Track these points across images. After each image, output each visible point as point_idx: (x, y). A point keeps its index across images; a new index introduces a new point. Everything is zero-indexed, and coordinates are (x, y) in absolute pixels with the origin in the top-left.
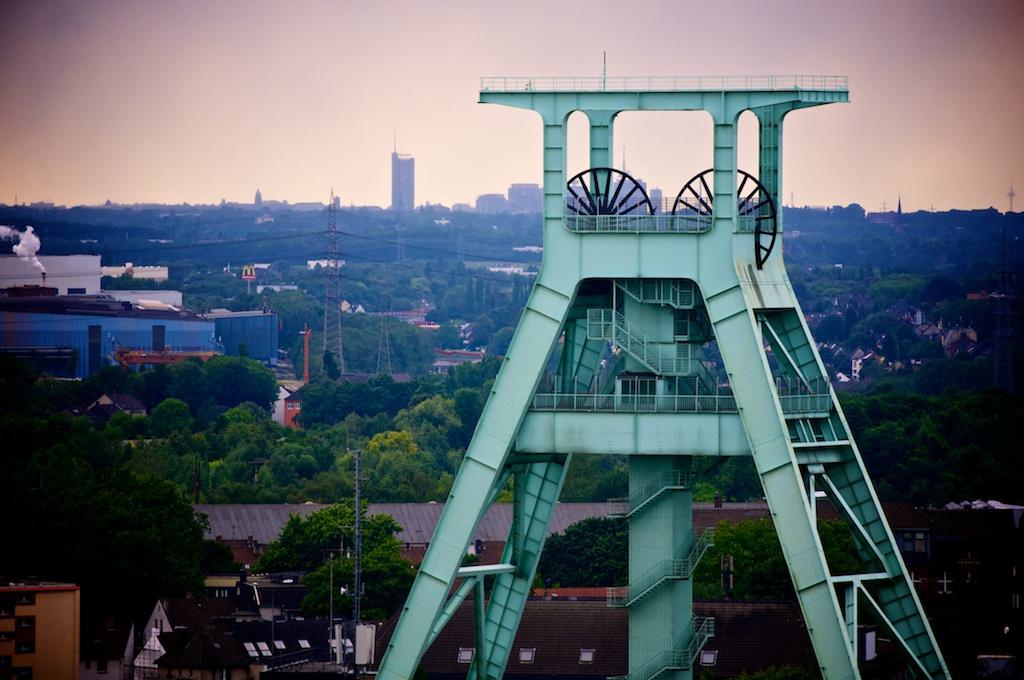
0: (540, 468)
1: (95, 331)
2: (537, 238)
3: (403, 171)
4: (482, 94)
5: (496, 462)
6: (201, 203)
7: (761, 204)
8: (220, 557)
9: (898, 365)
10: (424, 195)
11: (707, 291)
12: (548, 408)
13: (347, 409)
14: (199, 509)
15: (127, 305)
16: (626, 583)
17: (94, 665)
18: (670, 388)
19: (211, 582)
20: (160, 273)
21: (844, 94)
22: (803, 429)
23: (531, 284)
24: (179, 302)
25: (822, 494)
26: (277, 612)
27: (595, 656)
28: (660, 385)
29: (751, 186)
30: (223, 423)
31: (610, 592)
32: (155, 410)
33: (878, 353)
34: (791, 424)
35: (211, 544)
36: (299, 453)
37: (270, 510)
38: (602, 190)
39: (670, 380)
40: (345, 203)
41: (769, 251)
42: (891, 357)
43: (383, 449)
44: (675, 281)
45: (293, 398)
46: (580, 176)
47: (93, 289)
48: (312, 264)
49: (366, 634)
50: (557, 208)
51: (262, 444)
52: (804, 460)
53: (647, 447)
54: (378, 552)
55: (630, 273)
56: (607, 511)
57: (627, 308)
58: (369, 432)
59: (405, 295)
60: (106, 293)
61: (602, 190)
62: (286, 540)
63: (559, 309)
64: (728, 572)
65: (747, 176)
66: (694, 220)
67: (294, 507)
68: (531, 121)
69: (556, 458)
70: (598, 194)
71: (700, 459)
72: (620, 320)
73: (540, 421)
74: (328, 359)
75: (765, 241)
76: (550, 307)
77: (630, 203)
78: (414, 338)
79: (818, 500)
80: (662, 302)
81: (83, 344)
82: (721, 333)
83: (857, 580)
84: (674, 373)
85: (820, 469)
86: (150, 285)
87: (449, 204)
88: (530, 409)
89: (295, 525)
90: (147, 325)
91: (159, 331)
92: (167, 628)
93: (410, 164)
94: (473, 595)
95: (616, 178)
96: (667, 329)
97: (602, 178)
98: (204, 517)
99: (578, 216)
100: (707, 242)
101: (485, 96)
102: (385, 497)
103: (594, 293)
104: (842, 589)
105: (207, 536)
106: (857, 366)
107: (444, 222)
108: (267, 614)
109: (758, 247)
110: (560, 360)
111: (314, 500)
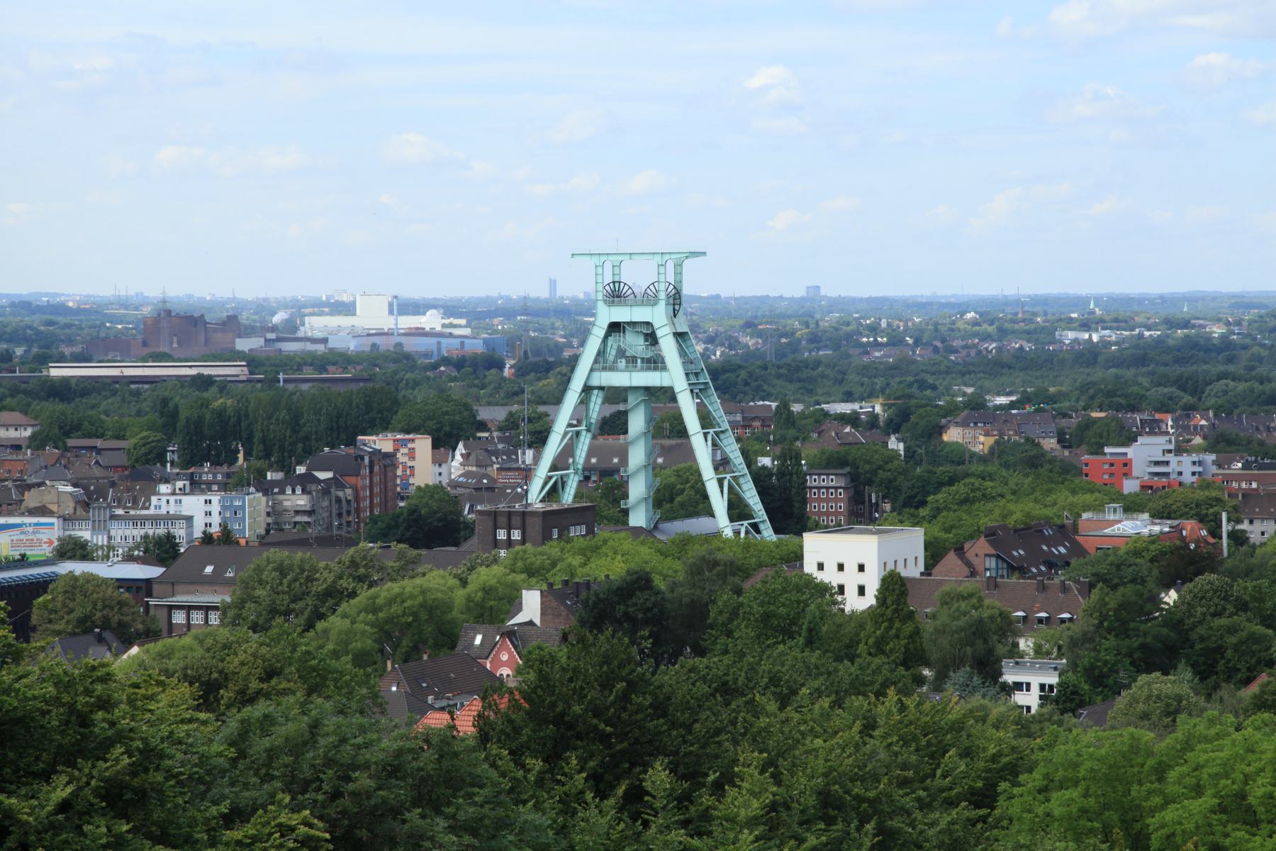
0: (595, 392)
1: (439, 343)
2: (595, 307)
3: (553, 283)
10: (559, 293)
11: (656, 326)
12: (598, 370)
13: (531, 371)
16: (626, 432)
18: (643, 362)
20: (463, 322)
21: (704, 254)
22: (692, 377)
28: (639, 361)
29: (671, 287)
30: (485, 376)
31: (622, 437)
34: (687, 374)
37: (501, 408)
39: (643, 359)
42: (731, 349)
44: (644, 323)
45: (511, 367)
47: (439, 328)
49: (530, 454)
50: (600, 296)
51: (500, 384)
53: (635, 384)
54: (541, 423)
56: (621, 407)
57: (627, 332)
58: (539, 379)
62: (507, 420)
63: (602, 333)
68: (590, 262)
69: (601, 388)
71: (655, 388)
73: (596, 374)
74: (525, 352)
76: (599, 332)
81: (435, 349)
82: (661, 341)
83: (711, 431)
86: (460, 326)
88: (592, 370)
89: (511, 415)
90: (458, 341)
91: (462, 343)
92: (464, 452)
93: (555, 281)
94: (571, 438)
95: (622, 285)
96: (641, 340)
97: (617, 285)
100: (655, 308)
101: (704, 254)
102: (545, 403)
103: (615, 327)
104: (705, 435)
105: (478, 418)
106: (718, 353)
108: (500, 446)
109: (674, 309)
110: (601, 353)
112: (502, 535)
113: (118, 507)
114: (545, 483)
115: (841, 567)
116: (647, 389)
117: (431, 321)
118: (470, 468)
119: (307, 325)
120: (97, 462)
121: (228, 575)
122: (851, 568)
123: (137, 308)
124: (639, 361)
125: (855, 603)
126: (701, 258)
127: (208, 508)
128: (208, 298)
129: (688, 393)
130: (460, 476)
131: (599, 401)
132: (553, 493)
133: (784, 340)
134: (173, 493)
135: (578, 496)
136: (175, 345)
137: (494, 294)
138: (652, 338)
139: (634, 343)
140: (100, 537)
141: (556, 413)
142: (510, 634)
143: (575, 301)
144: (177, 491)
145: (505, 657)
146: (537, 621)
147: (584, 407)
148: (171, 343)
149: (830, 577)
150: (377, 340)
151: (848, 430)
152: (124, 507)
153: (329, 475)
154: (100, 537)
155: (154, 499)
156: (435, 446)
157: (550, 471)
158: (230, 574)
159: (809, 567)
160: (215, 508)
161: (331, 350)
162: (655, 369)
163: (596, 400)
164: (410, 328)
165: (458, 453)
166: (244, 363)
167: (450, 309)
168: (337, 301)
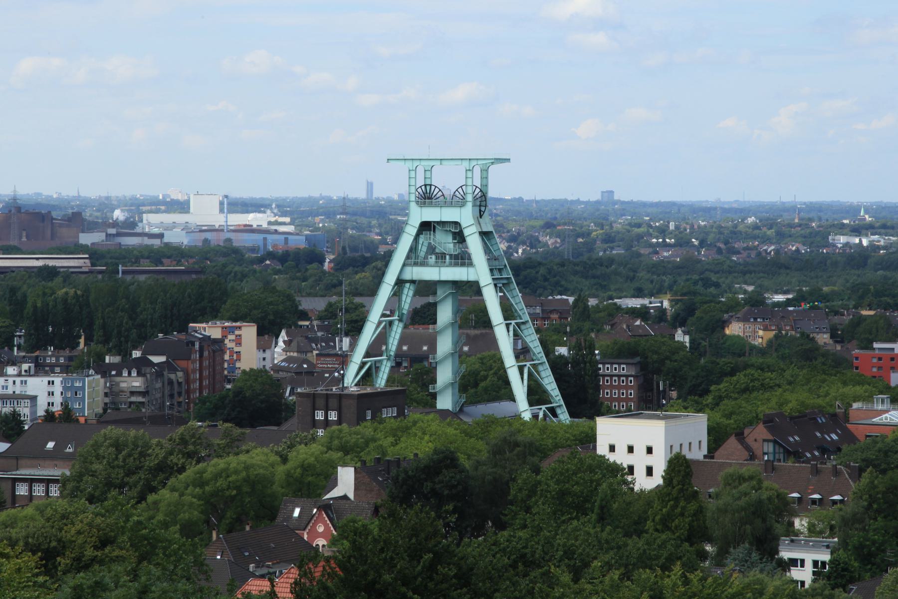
0: (407, 285)
1: (265, 239)
4: (388, 159)
5: (393, 283)
6: (328, 195)
7: (481, 196)
8: (304, 315)
9: (534, 251)
10: (376, 194)
11: (463, 225)
12: (410, 265)
14: (297, 299)
15: (276, 230)
16: (435, 322)
17: (261, 351)
19: (301, 323)
21: (508, 160)
22: (495, 272)
23: (406, 223)
24: (294, 229)
25: (502, 294)
26: (322, 333)
27: (428, 348)
28: (448, 257)
30: (307, 270)
32: (284, 266)
33: (527, 246)
35: (301, 311)
36: (332, 280)
37: (321, 299)
38: (428, 192)
39: (451, 255)
40: (591, 200)
41: (484, 212)
42: (532, 248)
43: (360, 278)
46: (421, 187)
48: (338, 217)
49: (346, 341)
50: (413, 198)
52: (496, 282)
53: (443, 278)
55: (438, 220)
56: (431, 299)
58: (356, 273)
59: (370, 227)
60: (269, 226)
61: (428, 192)
64: (472, 320)
65: (477, 187)
66: (457, 201)
67: (329, 298)
69: (413, 282)
70: (427, 193)
72: (434, 235)
73: (408, 269)
75: (483, 209)
76: (411, 231)
77: (438, 196)
78: (372, 242)
79: (500, 296)
80: (448, 229)
81: (261, 244)
82: (468, 240)
83: (513, 322)
84: (452, 253)
85: (501, 285)
86: (284, 224)
88: (404, 265)
89: (330, 305)
91: (286, 239)
92: (286, 339)
94: (385, 328)
95: (433, 188)
96: (450, 238)
97: (428, 188)
98: (299, 301)
99: (420, 200)
100: (463, 209)
101: (508, 160)
102: (361, 295)
103: (426, 227)
104: (508, 326)
106: (520, 251)
107: (383, 202)
108: (319, 334)
109: (480, 211)
110: (413, 250)
111: (336, 295)
115: (631, 449)
116: (456, 284)
118: (292, 354)
119: (145, 221)
122: (640, 450)
124: (448, 257)
128: (55, 196)
131: (411, 293)
132: (367, 377)
134: (19, 375)
136: (24, 239)
138: (459, 237)
139: (446, 243)
141: (371, 304)
142: (326, 507)
143: (390, 201)
144: (23, 373)
146: (351, 496)
148: (21, 237)
149: (621, 458)
151: (638, 323)
153: (162, 359)
156: (260, 333)
159: (602, 449)
160: (58, 388)
161: (167, 244)
162: (463, 265)
164: (239, 225)
166: (87, 256)
167: (283, 207)
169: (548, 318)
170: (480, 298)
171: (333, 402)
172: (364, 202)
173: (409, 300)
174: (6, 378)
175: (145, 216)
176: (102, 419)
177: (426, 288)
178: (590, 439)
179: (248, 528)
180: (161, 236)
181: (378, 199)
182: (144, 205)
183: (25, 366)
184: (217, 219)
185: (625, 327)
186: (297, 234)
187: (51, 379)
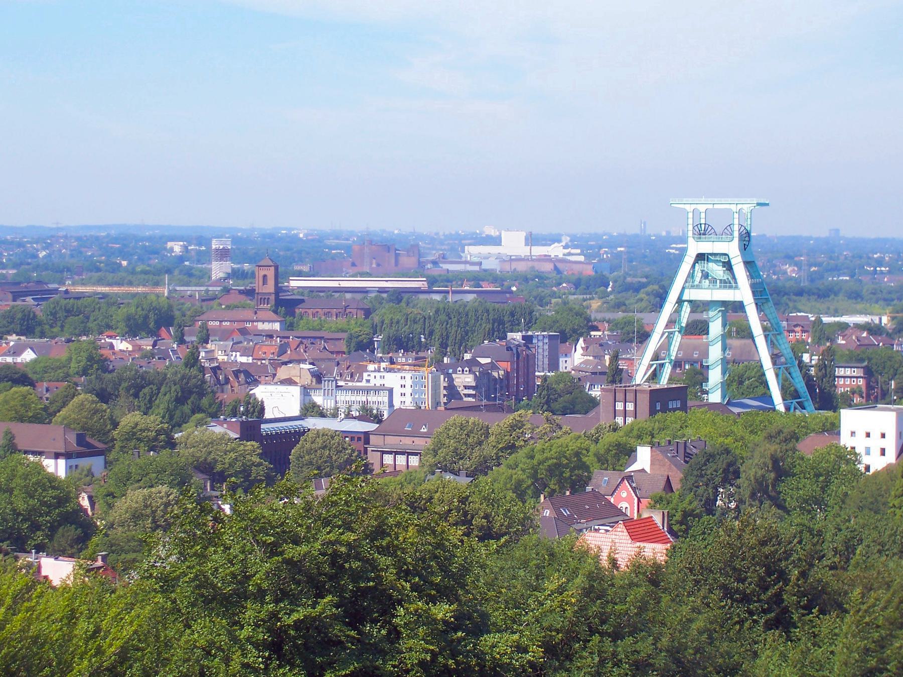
0: (686, 303)
10: (648, 232)
16: (707, 333)
20: (578, 251)
21: (768, 204)
28: (718, 281)
29: (743, 228)
39: (721, 280)
47: (561, 256)
53: (715, 299)
55: (711, 252)
63: (692, 261)
69: (690, 301)
83: (770, 334)
87: (814, 236)
88: (683, 288)
92: (583, 346)
103: (701, 257)
110: (691, 275)
112: (620, 406)
113: (341, 380)
114: (647, 370)
116: (724, 303)
117: (556, 251)
118: (588, 358)
119: (466, 252)
120: (325, 348)
121: (422, 430)
122: (876, 435)
123: (347, 239)
124: (718, 281)
125: (877, 463)
126: (765, 208)
127: (403, 382)
128: (396, 232)
129: (754, 306)
130: (581, 363)
131: (689, 310)
132: (654, 376)
133: (813, 269)
134: (379, 371)
135: (670, 379)
136: (374, 266)
137: (805, 234)
138: (728, 266)
139: (717, 270)
140: (329, 401)
141: (658, 318)
142: (629, 478)
143: (659, 237)
144: (382, 370)
145: (624, 495)
146: (648, 470)
147: (677, 314)
148: (371, 264)
150: (514, 265)
151: (865, 335)
152: (346, 380)
153: (488, 360)
154: (329, 401)
155: (365, 375)
157: (652, 360)
158: (424, 430)
160: (408, 382)
161: (485, 271)
162: (731, 287)
163: (686, 309)
164: (540, 255)
165: (578, 347)
166: (424, 279)
167: (577, 241)
168: (487, 236)
169: (793, 331)
170: (744, 314)
171: (630, 396)
172: (637, 236)
173: (687, 315)
174: (403, 375)
175: (466, 247)
176: (448, 406)
177: (697, 306)
178: (833, 429)
179: (568, 493)
180: (480, 264)
181: (650, 236)
182: (465, 239)
183: (383, 365)
184: (523, 251)
185: (854, 338)
186: (587, 264)
187: (403, 375)
